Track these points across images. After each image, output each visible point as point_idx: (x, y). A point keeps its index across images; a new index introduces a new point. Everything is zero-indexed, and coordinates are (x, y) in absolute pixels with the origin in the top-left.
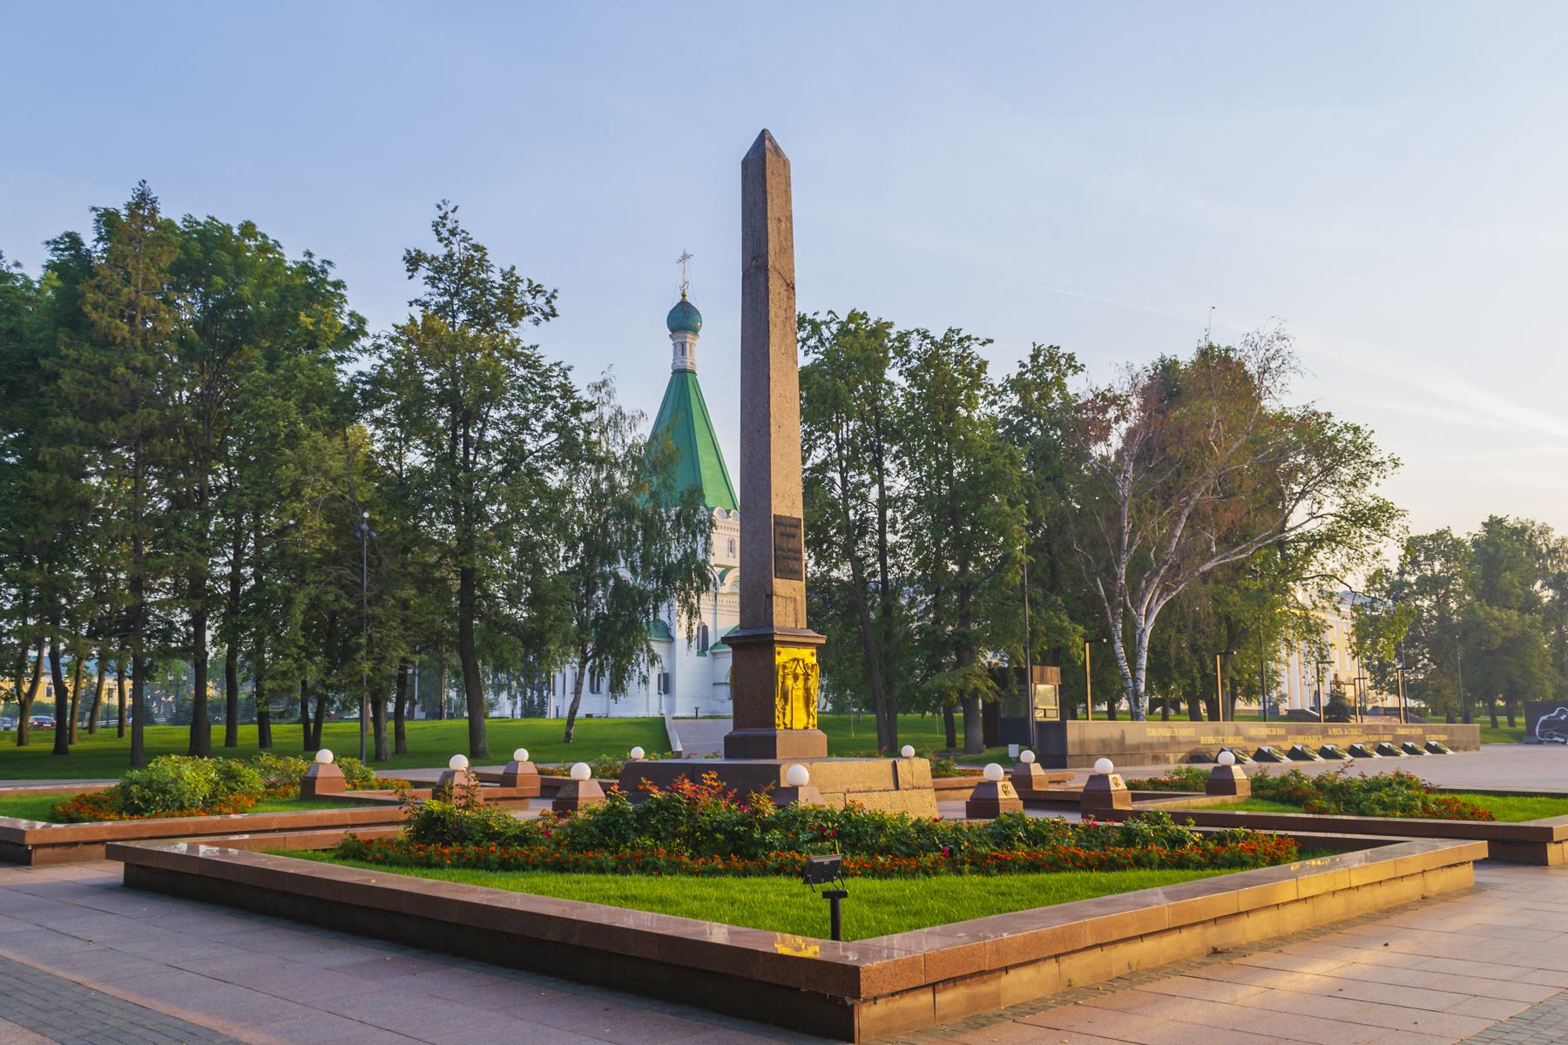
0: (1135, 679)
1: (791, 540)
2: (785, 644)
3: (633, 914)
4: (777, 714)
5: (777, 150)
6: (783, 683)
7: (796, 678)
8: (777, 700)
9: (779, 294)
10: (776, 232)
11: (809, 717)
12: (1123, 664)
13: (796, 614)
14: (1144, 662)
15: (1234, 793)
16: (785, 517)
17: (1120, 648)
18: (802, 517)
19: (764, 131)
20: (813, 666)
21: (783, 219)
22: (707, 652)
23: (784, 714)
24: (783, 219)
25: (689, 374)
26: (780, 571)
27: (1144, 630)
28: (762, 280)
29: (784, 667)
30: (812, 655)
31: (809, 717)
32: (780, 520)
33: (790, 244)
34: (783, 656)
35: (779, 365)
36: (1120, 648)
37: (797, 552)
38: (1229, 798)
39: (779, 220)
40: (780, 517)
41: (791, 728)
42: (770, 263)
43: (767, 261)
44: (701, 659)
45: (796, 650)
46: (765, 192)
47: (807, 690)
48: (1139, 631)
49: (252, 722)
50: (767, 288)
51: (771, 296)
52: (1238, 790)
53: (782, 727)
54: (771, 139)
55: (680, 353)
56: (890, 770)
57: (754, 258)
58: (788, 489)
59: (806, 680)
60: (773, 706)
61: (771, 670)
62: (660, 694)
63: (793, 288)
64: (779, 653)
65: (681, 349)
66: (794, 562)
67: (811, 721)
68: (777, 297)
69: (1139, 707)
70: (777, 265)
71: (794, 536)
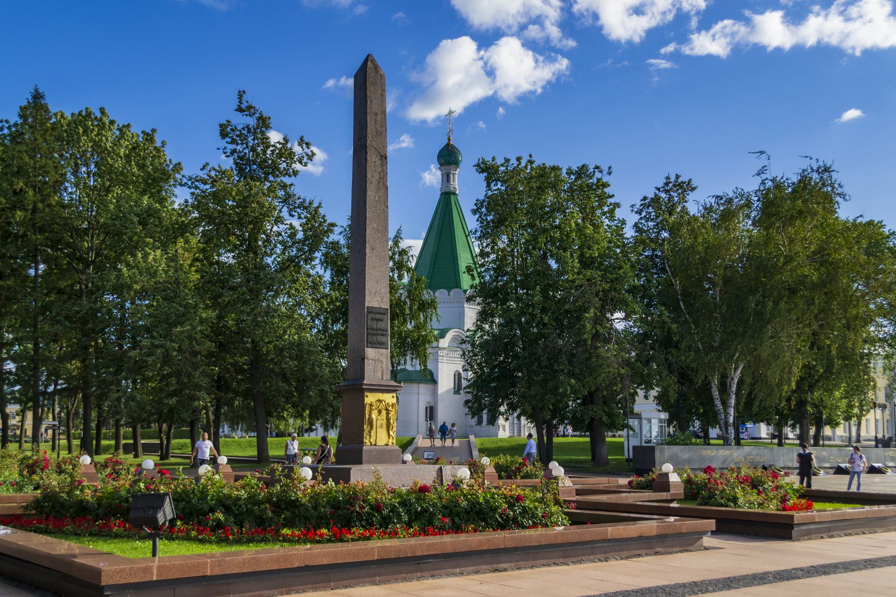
0: (727, 414)
1: (380, 322)
2: (372, 391)
3: (253, 554)
4: (365, 435)
5: (376, 67)
6: (370, 415)
7: (380, 412)
8: (365, 427)
9: (375, 162)
10: (373, 121)
11: (389, 437)
12: (718, 403)
13: (382, 371)
14: (733, 402)
15: (669, 491)
16: (376, 308)
17: (716, 394)
18: (388, 307)
19: (368, 55)
20: (393, 404)
21: (379, 113)
22: (461, 392)
23: (370, 436)
24: (379, 113)
25: (452, 197)
26: (370, 343)
27: (732, 379)
28: (364, 153)
29: (371, 405)
30: (393, 397)
31: (389, 437)
32: (371, 310)
33: (384, 129)
34: (370, 398)
35: (374, 209)
36: (716, 394)
37: (383, 331)
38: (664, 495)
39: (376, 114)
40: (372, 308)
41: (375, 445)
42: (368, 142)
43: (366, 141)
44: (457, 396)
45: (380, 394)
46: (366, 96)
47: (388, 419)
48: (729, 380)
49: (556, 443)
50: (366, 159)
51: (368, 164)
52: (671, 489)
53: (369, 444)
54: (373, 61)
55: (445, 180)
56: (861, 487)
57: (360, 139)
58: (378, 289)
59: (388, 414)
60: (363, 430)
61: (362, 406)
62: (427, 420)
63: (386, 158)
64: (367, 396)
65: (447, 178)
66: (382, 337)
67: (390, 441)
68: (373, 164)
69: (728, 434)
70: (374, 144)
71: (382, 320)
